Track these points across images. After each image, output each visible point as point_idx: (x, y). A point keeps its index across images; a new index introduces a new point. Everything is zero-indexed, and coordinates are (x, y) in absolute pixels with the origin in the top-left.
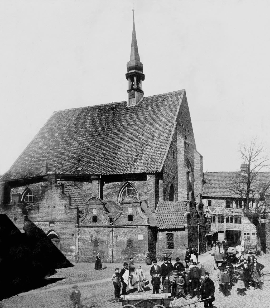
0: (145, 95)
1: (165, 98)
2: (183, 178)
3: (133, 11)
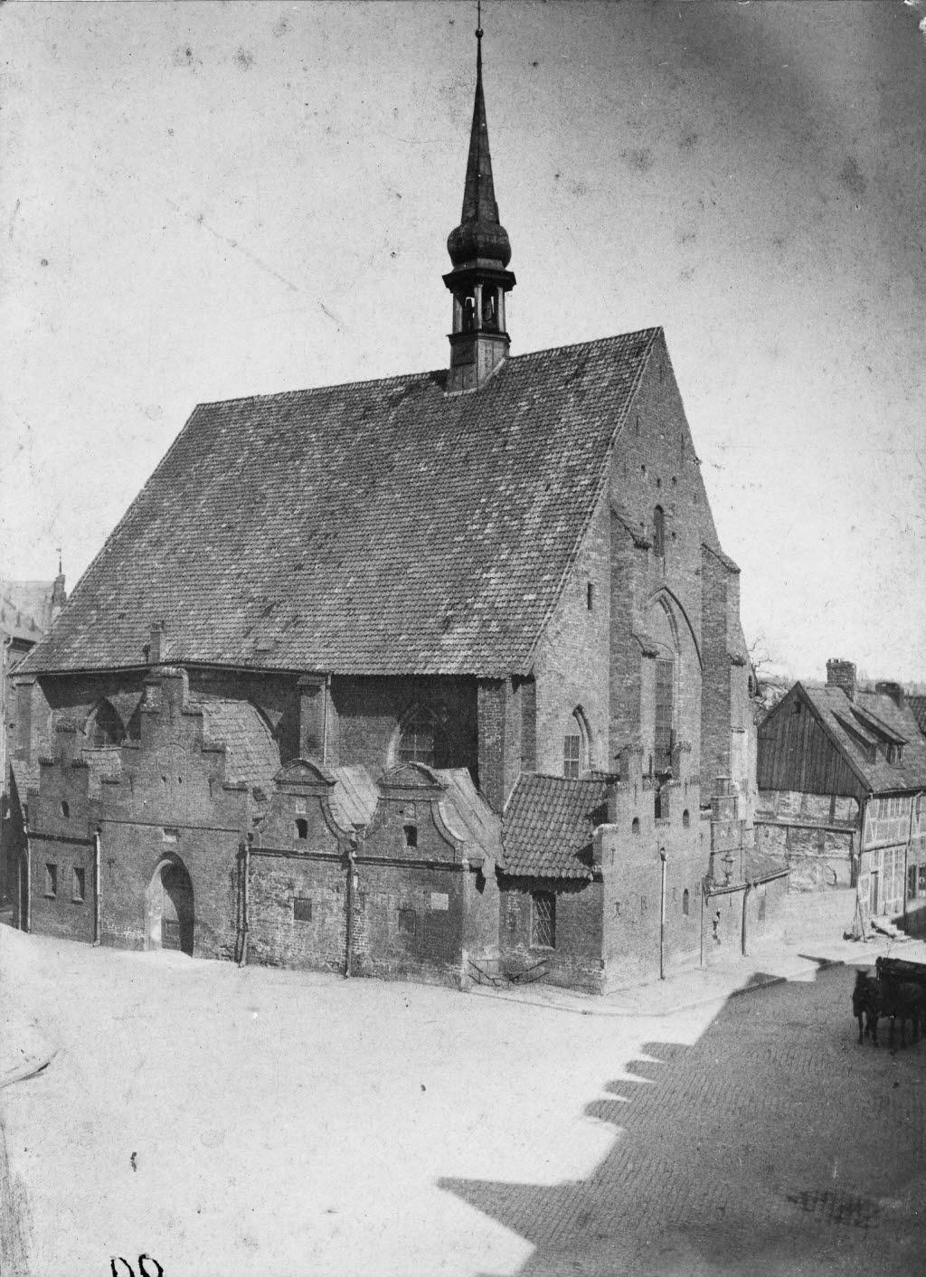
0: (515, 351)
1: (583, 366)
2: (628, 679)
3: (479, 34)
